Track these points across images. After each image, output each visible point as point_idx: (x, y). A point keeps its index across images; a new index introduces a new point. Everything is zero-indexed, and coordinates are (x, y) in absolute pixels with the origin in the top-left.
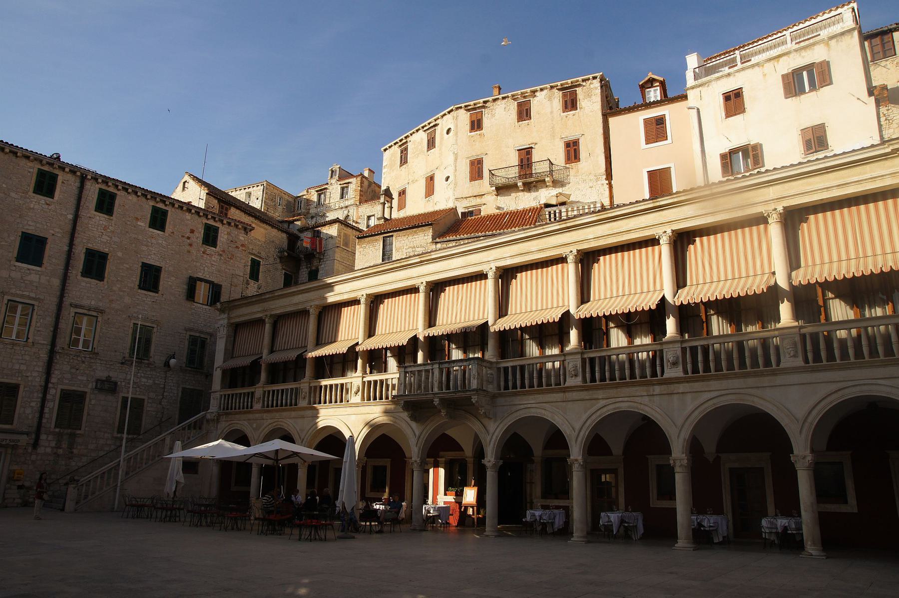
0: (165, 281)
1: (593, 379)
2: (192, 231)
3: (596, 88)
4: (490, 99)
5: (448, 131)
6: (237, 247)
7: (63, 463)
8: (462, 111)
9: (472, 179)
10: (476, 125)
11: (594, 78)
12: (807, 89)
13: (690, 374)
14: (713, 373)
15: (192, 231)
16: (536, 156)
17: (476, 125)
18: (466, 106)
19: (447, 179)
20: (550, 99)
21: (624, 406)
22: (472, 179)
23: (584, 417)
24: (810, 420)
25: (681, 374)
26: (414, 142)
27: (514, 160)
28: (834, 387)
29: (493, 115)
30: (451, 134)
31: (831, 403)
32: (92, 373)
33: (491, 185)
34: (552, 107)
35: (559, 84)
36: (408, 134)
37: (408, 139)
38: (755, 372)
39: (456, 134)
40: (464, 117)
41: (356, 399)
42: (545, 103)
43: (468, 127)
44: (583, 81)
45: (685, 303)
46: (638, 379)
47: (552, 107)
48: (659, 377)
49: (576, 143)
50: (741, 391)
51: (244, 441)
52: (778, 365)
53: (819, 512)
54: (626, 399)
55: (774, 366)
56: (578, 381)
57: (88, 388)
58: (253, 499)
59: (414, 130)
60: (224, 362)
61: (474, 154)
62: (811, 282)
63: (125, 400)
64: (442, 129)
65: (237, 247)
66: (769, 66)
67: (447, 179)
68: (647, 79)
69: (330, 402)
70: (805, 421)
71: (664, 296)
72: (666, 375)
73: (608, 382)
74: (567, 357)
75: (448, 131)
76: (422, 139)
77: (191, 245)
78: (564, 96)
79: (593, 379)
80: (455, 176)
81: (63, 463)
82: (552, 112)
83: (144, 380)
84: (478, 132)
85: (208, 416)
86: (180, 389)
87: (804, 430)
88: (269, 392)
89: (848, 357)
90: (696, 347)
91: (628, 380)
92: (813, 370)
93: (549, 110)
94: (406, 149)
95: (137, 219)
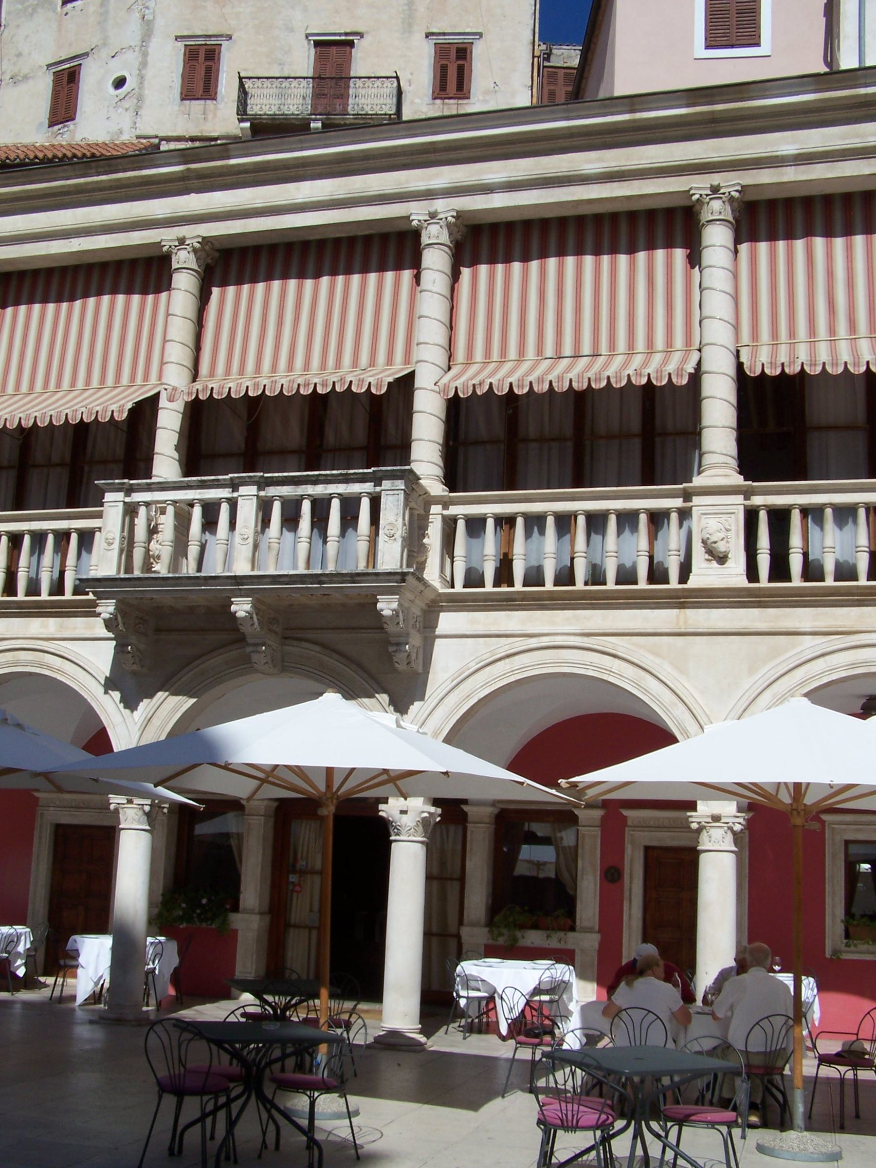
1: (780, 570)
9: (187, 95)
13: (764, 582)
14: (797, 582)
16: (362, 62)
19: (120, 83)
22: (187, 95)
25: (742, 582)
27: (303, 61)
28: (504, 646)
38: (813, 592)
46: (518, 587)
48: (674, 584)
49: (463, 53)
50: (46, 645)
52: (684, 577)
53: (382, 1002)
55: (674, 584)
56: (734, 575)
58: (45, 993)
67: (120, 83)
72: (694, 582)
74: (696, 500)
79: (780, 570)
80: (141, 78)
89: (787, 578)
90: (574, 515)
91: (489, 588)
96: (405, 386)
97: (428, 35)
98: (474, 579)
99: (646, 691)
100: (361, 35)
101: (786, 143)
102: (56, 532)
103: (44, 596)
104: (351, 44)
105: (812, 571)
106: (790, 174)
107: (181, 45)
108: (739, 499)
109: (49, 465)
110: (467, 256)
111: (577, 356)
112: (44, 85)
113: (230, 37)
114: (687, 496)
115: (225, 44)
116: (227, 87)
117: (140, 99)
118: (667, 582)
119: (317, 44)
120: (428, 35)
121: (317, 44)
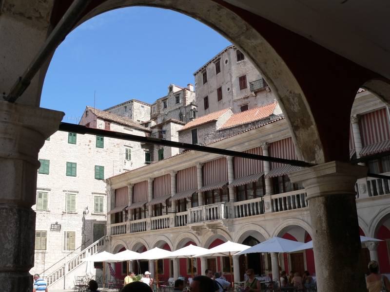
0: (79, 170)
2: (90, 141)
6: (114, 146)
7: (40, 266)
9: (241, 89)
15: (90, 141)
24: (373, 225)
26: (209, 69)
28: (382, 207)
30: (228, 63)
31: (381, 216)
32: (49, 221)
33: (252, 91)
37: (220, 57)
41: (172, 225)
43: (236, 59)
45: (238, 186)
51: (166, 247)
57: (48, 229)
60: (111, 209)
62: (383, 151)
63: (65, 232)
65: (114, 146)
69: (382, 193)
70: (371, 226)
73: (385, 194)
76: (213, 67)
77: (90, 149)
81: (40, 266)
83: (74, 222)
84: (242, 61)
85: (106, 238)
86: (93, 225)
87: (371, 230)
88: (213, 209)
92: (373, 199)
94: (206, 73)
95: (62, 140)
112: (216, 93)
116: (248, 85)
117: (232, 92)
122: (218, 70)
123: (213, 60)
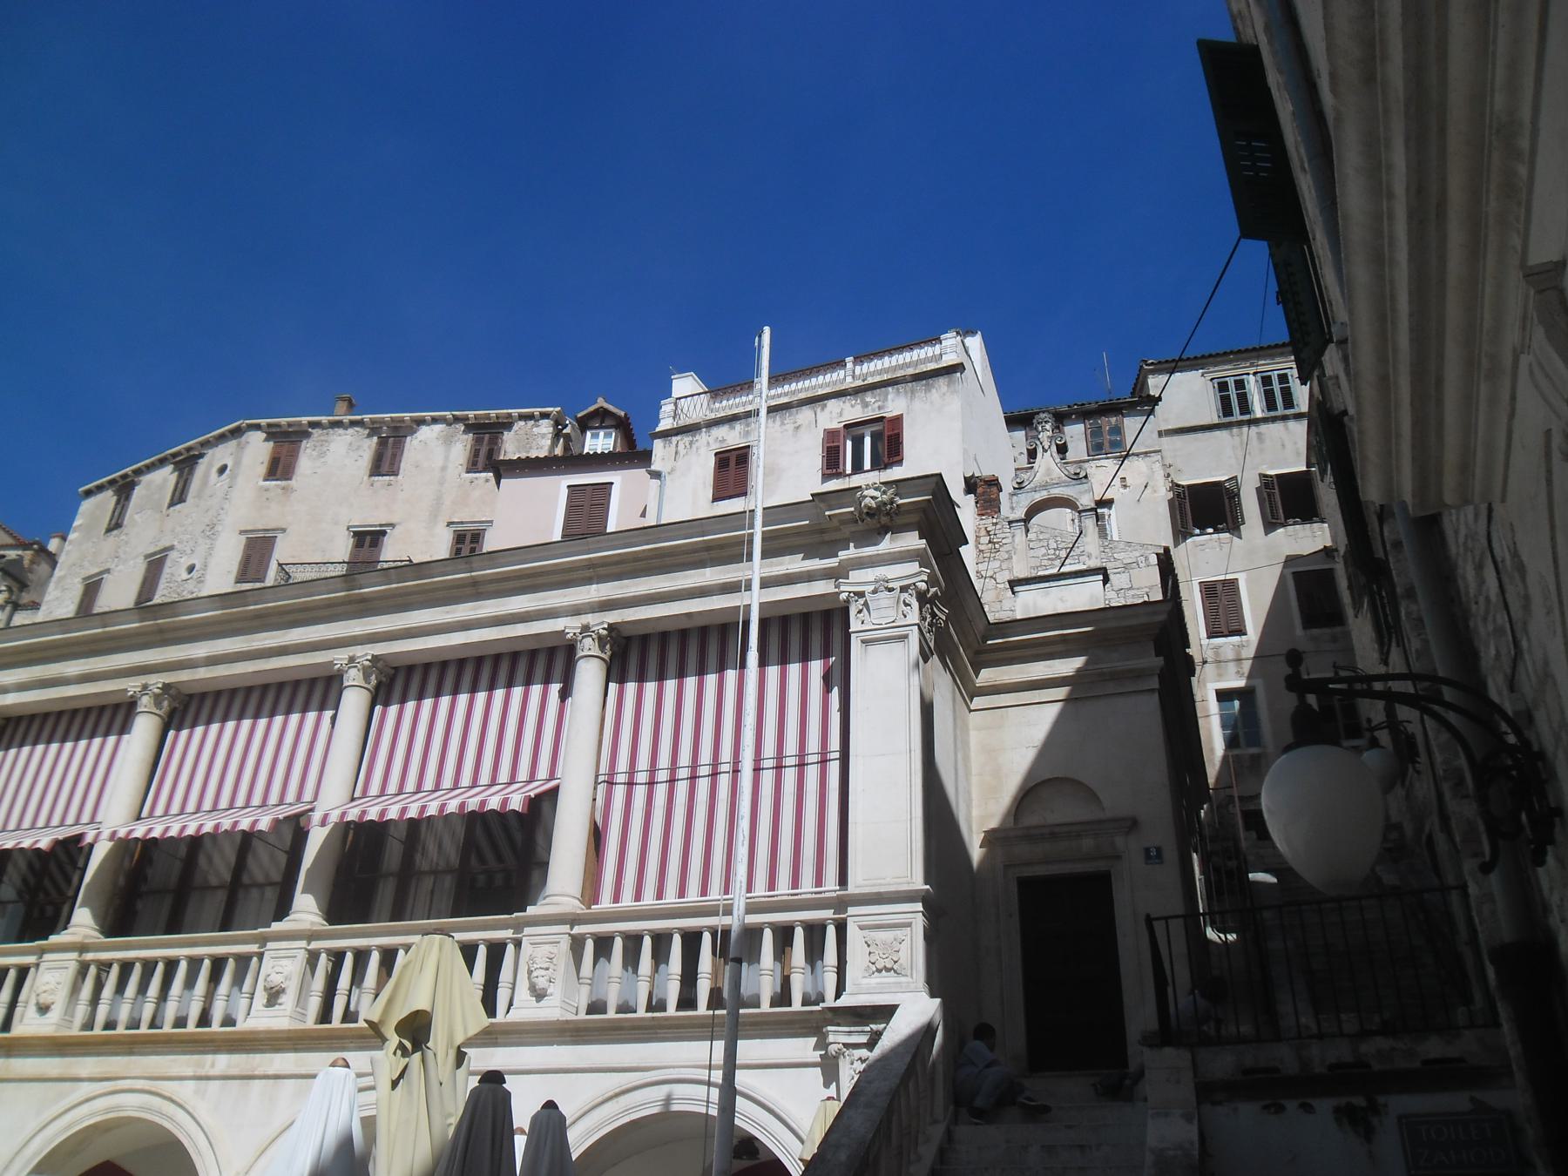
3: (543, 436)
4: (324, 419)
5: (222, 470)
8: (259, 436)
10: (280, 468)
11: (545, 416)
12: (867, 465)
17: (280, 468)
18: (269, 425)
19: (191, 569)
20: (448, 441)
21: (131, 1105)
23: (34, 1125)
27: (342, 548)
29: (322, 455)
34: (447, 458)
35: (471, 414)
36: (324, 419)
37: (316, 432)
39: (233, 477)
40: (257, 448)
42: (436, 449)
43: (262, 469)
44: (522, 417)
47: (447, 458)
54: (140, 1084)
59: (537, 411)
61: (370, 518)
64: (210, 465)
66: (805, 414)
67: (191, 569)
68: (592, 408)
71: (895, 1007)
75: (222, 470)
78: (478, 441)
82: (444, 468)
84: (283, 483)
93: (439, 462)
96: (542, 806)
97: (449, 524)
98: (656, 1005)
99: (36, 1154)
100: (392, 525)
101: (200, 650)
102: (329, 952)
103: (144, 1030)
104: (384, 533)
105: (349, 1016)
106: (203, 673)
107: (243, 538)
108: (566, 928)
109: (434, 872)
110: (176, 721)
111: (247, 805)
113: (284, 530)
114: (518, 927)
115: (280, 536)
118: (664, 1009)
119: (356, 534)
120: (449, 524)
121: (356, 534)
122: (179, 496)
123: (174, 455)
